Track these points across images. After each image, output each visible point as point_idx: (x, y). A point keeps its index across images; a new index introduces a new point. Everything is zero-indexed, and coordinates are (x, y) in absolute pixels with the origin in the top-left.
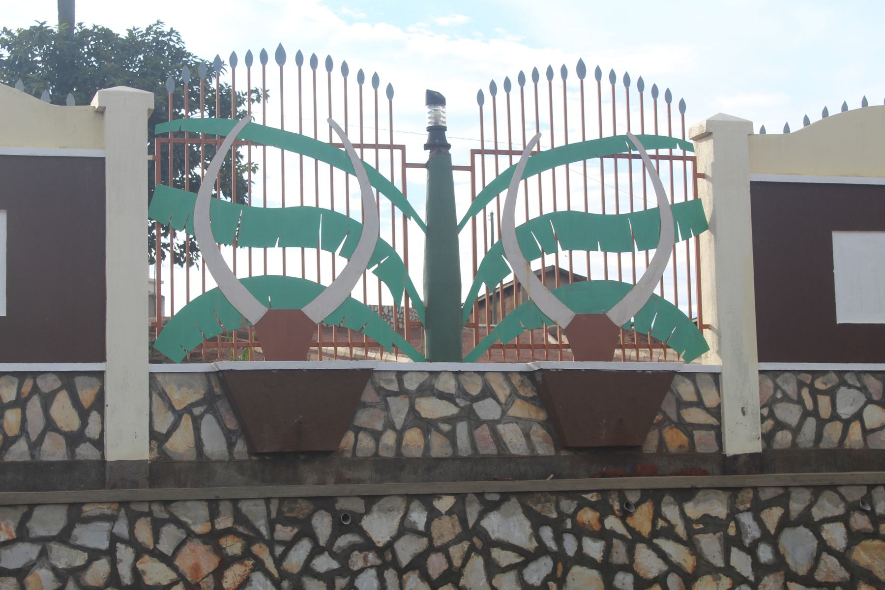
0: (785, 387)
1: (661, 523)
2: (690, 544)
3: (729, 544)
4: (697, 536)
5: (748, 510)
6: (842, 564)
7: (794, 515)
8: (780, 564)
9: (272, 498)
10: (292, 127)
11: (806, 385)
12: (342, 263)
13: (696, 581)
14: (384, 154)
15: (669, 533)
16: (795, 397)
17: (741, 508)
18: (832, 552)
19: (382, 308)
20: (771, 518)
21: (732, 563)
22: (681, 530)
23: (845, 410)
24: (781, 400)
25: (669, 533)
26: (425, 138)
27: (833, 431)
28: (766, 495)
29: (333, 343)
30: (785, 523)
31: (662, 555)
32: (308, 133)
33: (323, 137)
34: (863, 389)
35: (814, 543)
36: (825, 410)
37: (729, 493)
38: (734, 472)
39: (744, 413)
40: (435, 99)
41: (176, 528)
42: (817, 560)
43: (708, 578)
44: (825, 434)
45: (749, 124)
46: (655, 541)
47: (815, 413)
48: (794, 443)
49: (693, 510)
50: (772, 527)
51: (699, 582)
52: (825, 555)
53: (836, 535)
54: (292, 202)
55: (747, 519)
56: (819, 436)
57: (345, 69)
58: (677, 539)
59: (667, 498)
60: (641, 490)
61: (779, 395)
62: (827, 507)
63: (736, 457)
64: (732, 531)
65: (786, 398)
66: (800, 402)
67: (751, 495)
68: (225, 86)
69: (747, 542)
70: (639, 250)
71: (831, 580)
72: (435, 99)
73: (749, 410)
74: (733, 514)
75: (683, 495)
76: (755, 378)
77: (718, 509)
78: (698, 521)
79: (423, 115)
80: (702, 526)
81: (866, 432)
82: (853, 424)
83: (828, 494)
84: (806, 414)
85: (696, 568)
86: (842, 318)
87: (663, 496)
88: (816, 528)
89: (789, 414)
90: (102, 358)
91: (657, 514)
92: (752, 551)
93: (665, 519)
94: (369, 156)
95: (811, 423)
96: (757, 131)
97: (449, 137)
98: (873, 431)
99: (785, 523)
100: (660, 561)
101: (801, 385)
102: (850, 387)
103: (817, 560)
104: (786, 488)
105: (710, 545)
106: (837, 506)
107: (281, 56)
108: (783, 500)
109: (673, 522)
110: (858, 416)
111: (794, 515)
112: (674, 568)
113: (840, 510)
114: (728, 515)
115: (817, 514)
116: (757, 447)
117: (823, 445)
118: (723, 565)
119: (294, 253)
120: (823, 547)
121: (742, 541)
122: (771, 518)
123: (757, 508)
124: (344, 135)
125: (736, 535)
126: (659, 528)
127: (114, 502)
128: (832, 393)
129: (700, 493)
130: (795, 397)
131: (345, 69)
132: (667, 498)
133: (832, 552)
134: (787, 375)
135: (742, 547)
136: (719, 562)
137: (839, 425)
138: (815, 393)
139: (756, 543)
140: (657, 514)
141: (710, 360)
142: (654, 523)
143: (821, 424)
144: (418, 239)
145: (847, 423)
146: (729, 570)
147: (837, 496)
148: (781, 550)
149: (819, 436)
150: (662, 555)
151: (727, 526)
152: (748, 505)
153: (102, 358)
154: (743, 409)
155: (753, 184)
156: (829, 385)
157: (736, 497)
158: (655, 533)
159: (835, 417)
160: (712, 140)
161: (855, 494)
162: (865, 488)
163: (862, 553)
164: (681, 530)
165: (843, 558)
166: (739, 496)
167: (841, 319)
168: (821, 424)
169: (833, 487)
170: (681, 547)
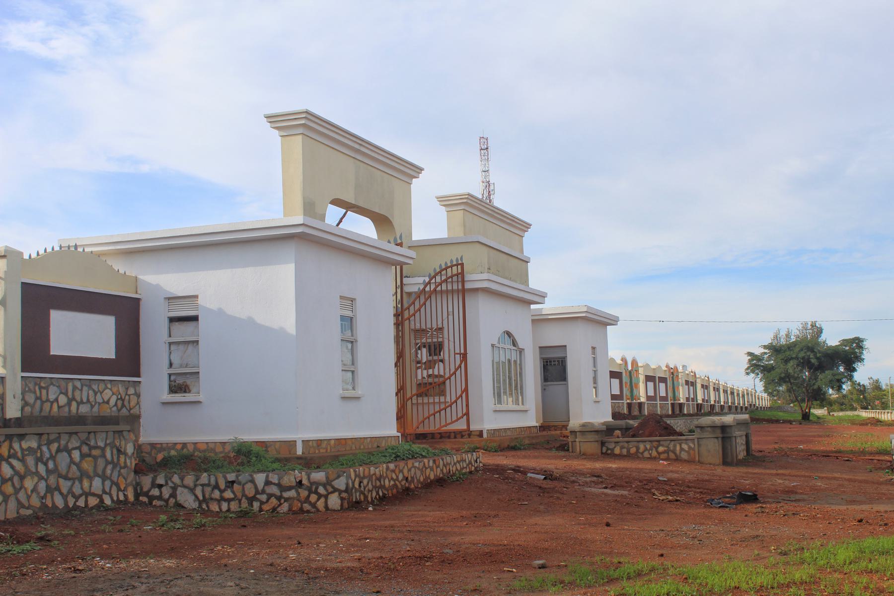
0: (30, 385)
1: (12, 451)
2: (23, 461)
3: (39, 460)
4: (26, 457)
5: (45, 444)
6: (78, 469)
7: (62, 447)
8: (56, 470)
9: (27, 434)
11: (37, 384)
13: (25, 479)
15: (14, 456)
16: (33, 390)
17: (43, 443)
18: (75, 463)
20: (54, 447)
21: (39, 470)
22: (20, 454)
23: (52, 397)
24: (28, 391)
25: (14, 456)
27: (47, 406)
28: (52, 437)
30: (59, 450)
31: (12, 467)
34: (59, 387)
35: (68, 460)
36: (44, 398)
37: (38, 436)
38: (9, 427)
39: (14, 398)
42: (69, 467)
43: (29, 477)
44: (44, 409)
45: (22, 253)
46: (10, 460)
47: (40, 398)
48: (32, 413)
49: (25, 445)
50: (54, 452)
51: (26, 479)
52: (72, 465)
53: (76, 455)
55: (45, 448)
56: (41, 410)
58: (18, 459)
59: (15, 439)
60: (6, 435)
61: (27, 389)
62: (74, 443)
63: (10, 419)
64: (39, 455)
65: (30, 391)
66: (35, 392)
67: (47, 437)
69: (45, 459)
71: (74, 477)
73: (17, 396)
74: (39, 447)
75: (22, 437)
76: (19, 379)
77: (34, 444)
78: (26, 450)
80: (27, 452)
81: (59, 407)
82: (54, 404)
83: (74, 436)
84: (37, 398)
85: (25, 473)
86: (53, 352)
87: (13, 438)
88: (69, 452)
89: (30, 398)
91: (11, 447)
92: (46, 464)
93: (14, 449)
95: (39, 402)
96: (26, 257)
98: (62, 407)
99: (59, 450)
100: (11, 470)
101: (36, 384)
102: (54, 385)
103: (69, 467)
104: (59, 433)
105: (30, 461)
106: (77, 442)
108: (58, 439)
109: (17, 451)
110: (57, 400)
111: (62, 447)
112: (17, 473)
113: (78, 445)
114: (37, 447)
115: (70, 446)
116: (18, 414)
117: (43, 414)
118: (35, 471)
120: (72, 461)
121: (42, 459)
122: (54, 447)
123: (49, 443)
125: (40, 457)
126: (11, 453)
127: (114, 436)
128: (47, 388)
129: (27, 436)
130: (33, 390)
132: (15, 439)
133: (75, 463)
134: (31, 379)
135: (42, 462)
136: (34, 470)
137: (49, 404)
138: (41, 388)
139: (48, 460)
140: (11, 447)
142: (9, 452)
143: (43, 402)
145: (52, 403)
146: (37, 473)
147: (77, 437)
148: (57, 463)
149: (41, 410)
150: (12, 467)
151: (37, 452)
152: (46, 442)
153: (139, 376)
154: (14, 395)
155: (23, 283)
156: (46, 385)
157: (41, 438)
158: (10, 456)
159: (48, 400)
160: (6, 260)
161: (84, 436)
162: (87, 433)
163: (85, 464)
164: (20, 454)
165: (78, 465)
166: (42, 437)
167: (53, 352)
168: (43, 402)
169: (76, 433)
170: (20, 463)
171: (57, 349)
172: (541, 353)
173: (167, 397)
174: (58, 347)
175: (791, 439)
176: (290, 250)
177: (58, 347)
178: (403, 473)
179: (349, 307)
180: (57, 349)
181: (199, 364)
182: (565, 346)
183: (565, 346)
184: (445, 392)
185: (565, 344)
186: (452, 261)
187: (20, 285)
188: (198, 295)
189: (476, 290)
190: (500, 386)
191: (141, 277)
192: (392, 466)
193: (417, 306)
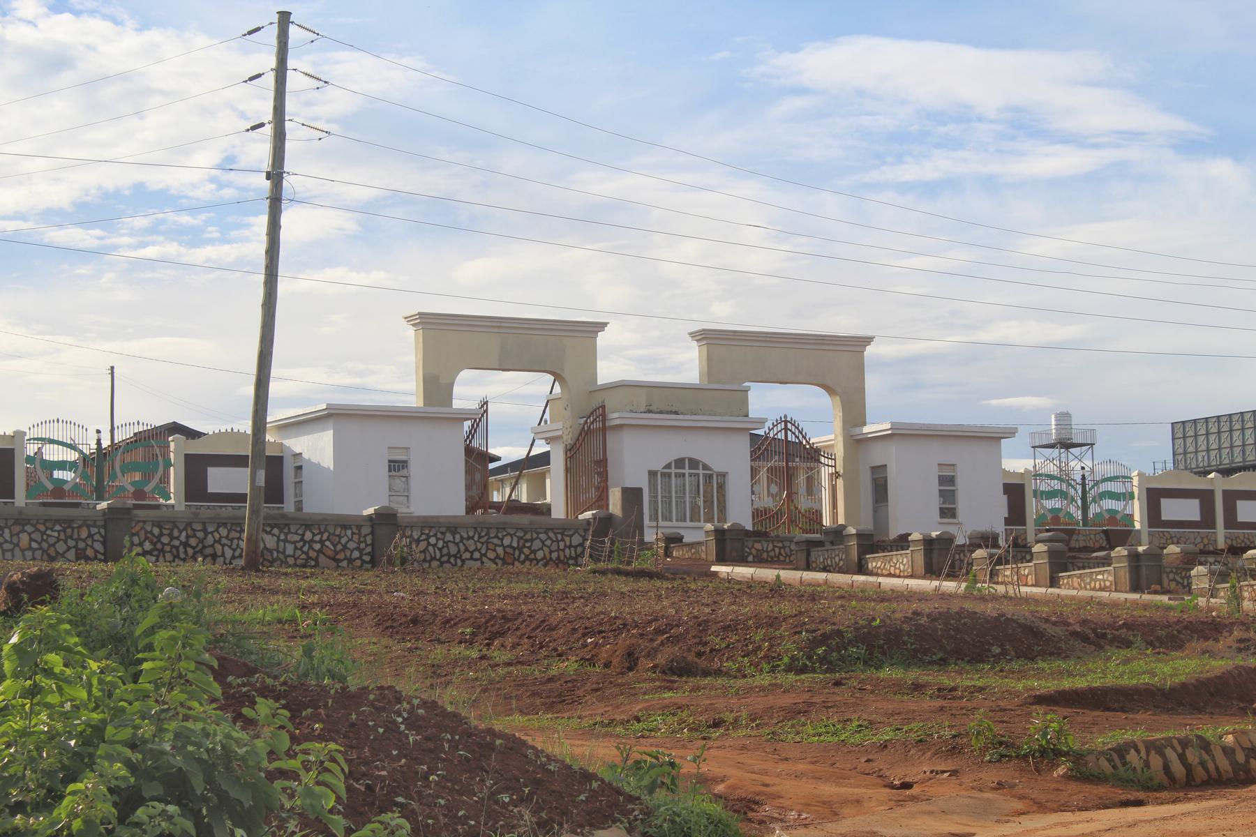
10: (60, 440)
12: (73, 475)
14: (85, 446)
19: (1255, 427)
26: (95, 442)
29: (864, 424)
32: (65, 441)
33: (69, 442)
40: (98, 432)
41: (322, 464)
54: (61, 459)
57: (75, 424)
68: (1081, 655)
70: (641, 490)
72: (98, 432)
79: (95, 436)
86: (1163, 519)
90: (14, 498)
94: (81, 447)
97: (102, 442)
107: (58, 421)
119: (61, 472)
124: (74, 441)
131: (75, 424)
141: (172, 502)
144: (1080, 512)
153: (14, 498)
167: (1163, 519)
171: (1164, 517)
172: (873, 473)
173: (939, 520)
174: (1165, 516)
175: (801, 767)
176: (330, 423)
177: (1165, 516)
178: (322, 536)
179: (44, 430)
180: (1164, 517)
181: (390, 481)
182: (886, 465)
183: (886, 465)
184: (944, 518)
185: (884, 463)
186: (777, 421)
187: (1002, 485)
188: (1147, 489)
189: (620, 427)
190: (670, 497)
191: (284, 442)
192: (693, 550)
193: (578, 446)
